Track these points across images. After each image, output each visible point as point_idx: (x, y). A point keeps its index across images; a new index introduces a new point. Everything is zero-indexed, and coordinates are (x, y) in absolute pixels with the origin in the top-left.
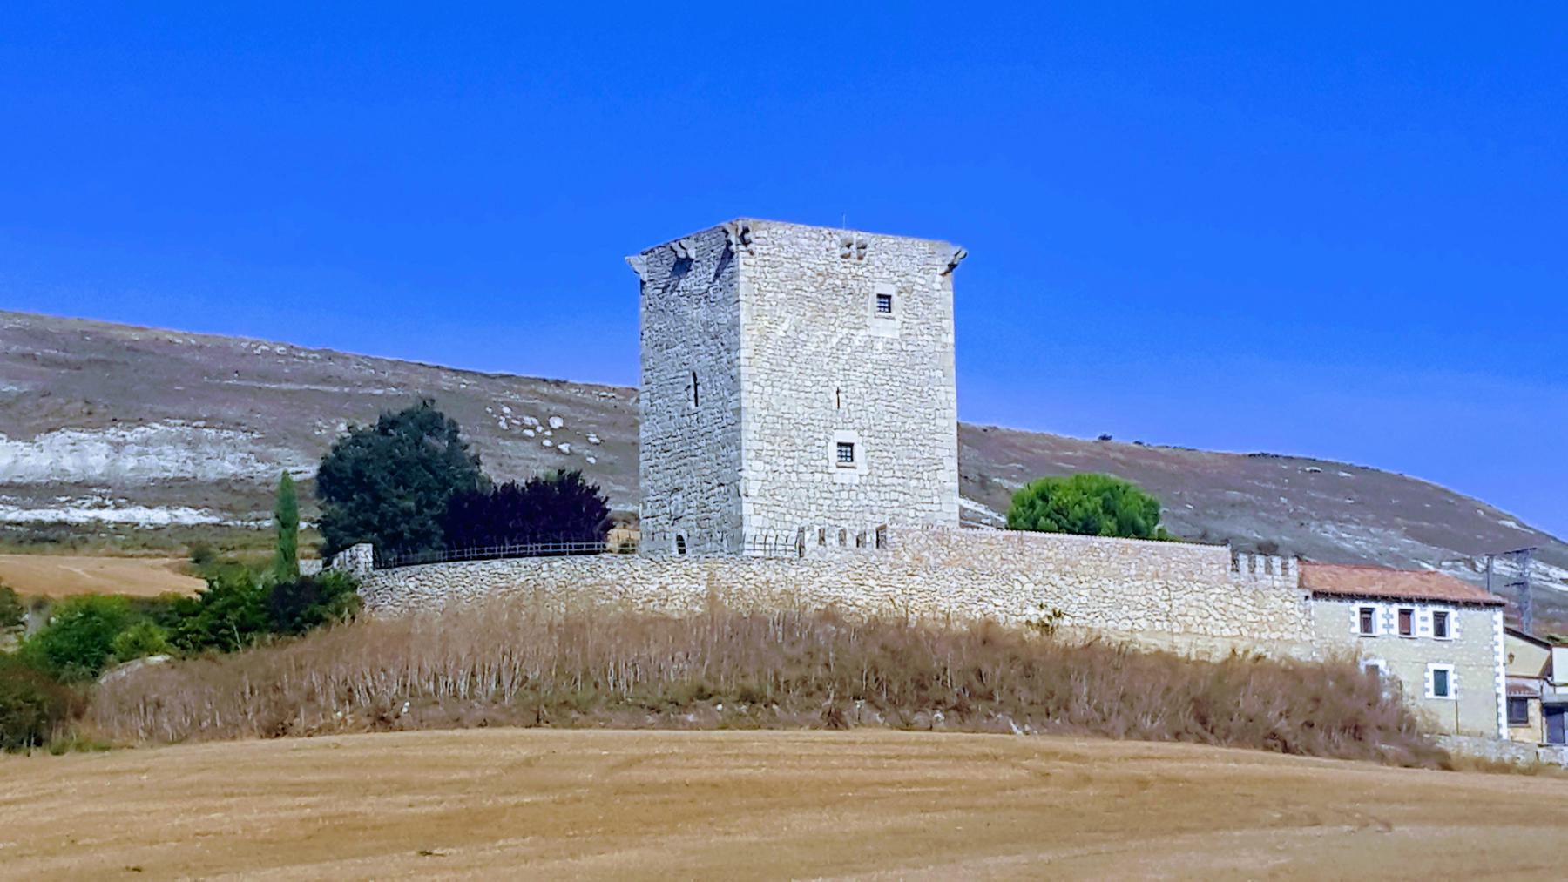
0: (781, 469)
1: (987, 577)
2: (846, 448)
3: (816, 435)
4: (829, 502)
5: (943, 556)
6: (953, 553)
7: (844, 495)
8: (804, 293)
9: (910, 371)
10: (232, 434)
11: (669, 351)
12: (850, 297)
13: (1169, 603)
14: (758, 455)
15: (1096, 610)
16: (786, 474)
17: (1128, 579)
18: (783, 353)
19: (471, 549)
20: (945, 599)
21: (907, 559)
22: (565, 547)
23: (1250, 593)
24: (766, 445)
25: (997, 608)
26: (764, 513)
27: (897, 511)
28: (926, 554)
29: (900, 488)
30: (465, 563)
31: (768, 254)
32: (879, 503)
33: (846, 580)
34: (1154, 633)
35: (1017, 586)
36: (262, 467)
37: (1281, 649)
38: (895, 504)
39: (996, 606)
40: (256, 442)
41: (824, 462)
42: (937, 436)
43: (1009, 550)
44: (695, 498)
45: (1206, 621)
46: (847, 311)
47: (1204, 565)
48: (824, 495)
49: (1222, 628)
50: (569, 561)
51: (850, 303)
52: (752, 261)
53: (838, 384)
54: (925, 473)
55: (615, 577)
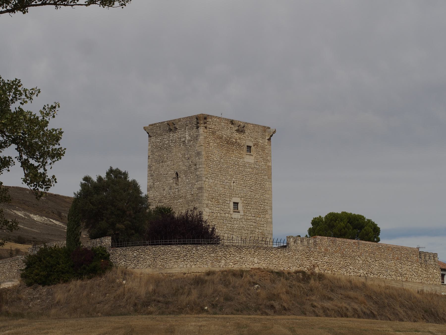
0: (215, 211)
1: (348, 258)
2: (236, 204)
3: (226, 199)
5: (334, 249)
6: (337, 248)
7: (235, 222)
8: (223, 144)
9: (257, 176)
12: (238, 146)
13: (401, 269)
14: (207, 206)
15: (380, 272)
20: (335, 266)
22: (202, 241)
23: (424, 266)
24: (210, 202)
27: (252, 229)
28: (329, 248)
29: (254, 221)
31: (211, 128)
33: (304, 258)
34: (396, 281)
35: (357, 261)
38: (252, 227)
39: (351, 269)
41: (229, 209)
42: (266, 201)
43: (355, 247)
46: (237, 151)
47: (411, 255)
48: (229, 222)
49: (416, 279)
50: (204, 247)
52: (206, 130)
54: (262, 215)
55: (223, 254)
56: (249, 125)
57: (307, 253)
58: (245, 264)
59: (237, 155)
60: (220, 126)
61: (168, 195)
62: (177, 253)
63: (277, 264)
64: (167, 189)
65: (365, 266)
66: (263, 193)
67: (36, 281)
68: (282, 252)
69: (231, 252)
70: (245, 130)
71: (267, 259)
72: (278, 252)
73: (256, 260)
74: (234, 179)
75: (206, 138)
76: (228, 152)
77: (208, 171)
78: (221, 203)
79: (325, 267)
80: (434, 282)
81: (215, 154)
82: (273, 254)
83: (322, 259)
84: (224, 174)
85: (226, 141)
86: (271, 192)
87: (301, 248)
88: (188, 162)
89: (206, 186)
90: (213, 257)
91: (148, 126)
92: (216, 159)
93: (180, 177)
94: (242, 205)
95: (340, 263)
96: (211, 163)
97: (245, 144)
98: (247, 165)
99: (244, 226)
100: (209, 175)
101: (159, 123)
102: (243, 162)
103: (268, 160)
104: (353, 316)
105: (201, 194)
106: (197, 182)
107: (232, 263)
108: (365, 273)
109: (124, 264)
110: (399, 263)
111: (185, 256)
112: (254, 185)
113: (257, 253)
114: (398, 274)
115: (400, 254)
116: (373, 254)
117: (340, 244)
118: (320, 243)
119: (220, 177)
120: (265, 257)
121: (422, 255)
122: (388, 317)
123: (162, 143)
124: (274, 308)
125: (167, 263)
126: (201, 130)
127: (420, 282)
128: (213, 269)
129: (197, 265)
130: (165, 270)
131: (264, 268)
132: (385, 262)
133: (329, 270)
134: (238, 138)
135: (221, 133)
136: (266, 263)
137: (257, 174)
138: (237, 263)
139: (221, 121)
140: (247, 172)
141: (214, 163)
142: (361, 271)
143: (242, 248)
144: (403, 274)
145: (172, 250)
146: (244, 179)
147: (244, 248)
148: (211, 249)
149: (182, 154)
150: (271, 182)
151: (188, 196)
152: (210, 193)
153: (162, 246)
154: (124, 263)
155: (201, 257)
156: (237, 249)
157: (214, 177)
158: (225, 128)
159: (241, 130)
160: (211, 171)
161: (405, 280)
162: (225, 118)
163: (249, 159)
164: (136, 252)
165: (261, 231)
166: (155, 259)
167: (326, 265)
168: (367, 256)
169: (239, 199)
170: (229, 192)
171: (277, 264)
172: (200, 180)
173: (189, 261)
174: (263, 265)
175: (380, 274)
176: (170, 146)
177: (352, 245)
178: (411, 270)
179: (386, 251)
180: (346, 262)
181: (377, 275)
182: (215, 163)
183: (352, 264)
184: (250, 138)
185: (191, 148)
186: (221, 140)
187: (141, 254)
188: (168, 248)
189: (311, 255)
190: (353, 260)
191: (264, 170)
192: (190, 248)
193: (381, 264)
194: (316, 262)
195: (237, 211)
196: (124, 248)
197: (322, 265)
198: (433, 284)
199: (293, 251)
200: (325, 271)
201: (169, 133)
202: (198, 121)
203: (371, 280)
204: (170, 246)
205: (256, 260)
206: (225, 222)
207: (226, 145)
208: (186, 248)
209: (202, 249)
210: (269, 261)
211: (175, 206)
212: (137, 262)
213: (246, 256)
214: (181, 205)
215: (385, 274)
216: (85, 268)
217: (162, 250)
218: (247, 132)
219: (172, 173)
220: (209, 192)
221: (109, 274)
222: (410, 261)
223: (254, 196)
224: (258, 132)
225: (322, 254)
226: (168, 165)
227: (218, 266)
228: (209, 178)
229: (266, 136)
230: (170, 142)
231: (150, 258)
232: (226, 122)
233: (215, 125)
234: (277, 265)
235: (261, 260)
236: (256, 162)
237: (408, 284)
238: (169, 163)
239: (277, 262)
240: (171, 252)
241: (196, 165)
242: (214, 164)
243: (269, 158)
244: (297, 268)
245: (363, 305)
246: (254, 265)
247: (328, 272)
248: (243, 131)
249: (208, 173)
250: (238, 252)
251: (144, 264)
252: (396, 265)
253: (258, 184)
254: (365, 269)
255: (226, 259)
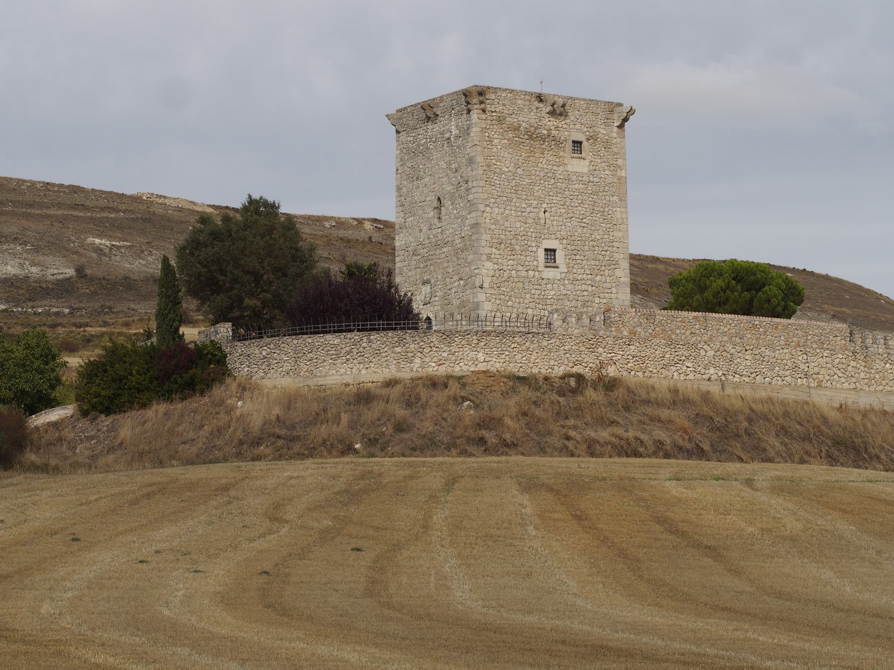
0: (505, 268)
1: (682, 346)
2: (550, 253)
3: (529, 243)
4: (539, 292)
5: (650, 331)
6: (657, 329)
7: (550, 286)
8: (520, 140)
9: (595, 197)
10: (12, 246)
11: (419, 182)
12: (553, 142)
13: (807, 365)
14: (489, 257)
15: (756, 371)
16: (508, 271)
17: (779, 348)
18: (506, 183)
19: (309, 326)
20: (652, 362)
21: (625, 333)
23: (862, 357)
24: (494, 250)
25: (689, 369)
26: (493, 300)
27: (586, 298)
29: (589, 282)
30: (304, 336)
32: (574, 293)
33: (582, 349)
34: (796, 387)
35: (703, 353)
36: (34, 270)
37: (802, 396)
38: (585, 293)
39: (688, 367)
40: (27, 251)
41: (535, 263)
42: (615, 244)
44: (440, 289)
45: (832, 378)
46: (551, 153)
47: (831, 337)
48: (536, 287)
49: (843, 383)
50: (382, 335)
51: (553, 147)
52: (484, 116)
53: (545, 205)
54: (607, 271)
55: (417, 346)
56: (576, 101)
57: (590, 340)
58: (460, 364)
59: (551, 159)
60: (515, 106)
61: (426, 240)
62: (335, 349)
63: (525, 362)
64: (425, 229)
65: (721, 360)
66: (609, 230)
67: (94, 407)
68: (536, 339)
69: (432, 344)
70: (568, 111)
71: (504, 353)
72: (526, 340)
73: (481, 356)
74: (545, 205)
75: (484, 131)
76: (532, 154)
77: (489, 192)
78: (519, 252)
79: (630, 365)
80: (885, 387)
81: (504, 159)
82: (516, 344)
83: (623, 351)
84: (524, 197)
85: (528, 133)
86: (625, 226)
87: (576, 331)
88: (456, 177)
89: (487, 220)
90: (399, 353)
91: (395, 112)
92: (507, 170)
93: (444, 206)
94: (563, 253)
95: (664, 357)
96: (495, 178)
97: (568, 138)
98: (574, 178)
99: (569, 293)
100: (493, 200)
101: (412, 106)
102: (565, 172)
103: (619, 167)
104: (655, 454)
105: (476, 235)
106: (469, 214)
107: (435, 362)
108: (720, 373)
109: (248, 371)
110: (801, 353)
111: (348, 353)
112: (588, 214)
113: (483, 344)
114: (798, 374)
115: (803, 336)
116: (740, 338)
117: (663, 322)
118: (620, 321)
119: (515, 203)
120: (499, 349)
121: (857, 336)
122: (736, 455)
123: (416, 143)
124: (486, 442)
125: (317, 367)
126: (475, 115)
127: (852, 387)
128: (399, 375)
129: (371, 370)
130: (314, 379)
131: (497, 371)
132: (767, 352)
133: (639, 370)
134: (552, 128)
135: (516, 120)
136: (502, 361)
137: (596, 193)
138: (444, 362)
139: (517, 97)
140: (575, 190)
141: (503, 176)
142: (712, 371)
143: (454, 335)
144: (811, 373)
145: (327, 342)
146: (568, 204)
147: (457, 335)
148: (396, 340)
149: (446, 163)
150: (626, 207)
151: (457, 241)
152: (495, 233)
153: (308, 336)
154: (247, 369)
155: (377, 353)
156: (444, 337)
157: (502, 202)
158: (526, 110)
159: (559, 111)
160: (496, 191)
161: (816, 384)
162: (526, 92)
163: (579, 166)
164: (265, 348)
165: (605, 301)
166: (296, 361)
167: (632, 361)
168: (725, 341)
169: (557, 242)
170: (535, 230)
171: (525, 362)
172: (474, 209)
173: (355, 361)
174: (496, 365)
175: (757, 375)
176: (428, 148)
177: (691, 321)
178: (831, 366)
179: (770, 330)
180: (676, 354)
181: (749, 377)
182: (505, 177)
183: (691, 357)
184: (578, 126)
185: (460, 151)
186: (516, 132)
187: (274, 353)
188: (319, 339)
189: (599, 344)
190: (693, 350)
191: (610, 186)
192: (358, 337)
193: (758, 357)
194: (609, 355)
195: (552, 265)
196: (247, 343)
197: (623, 362)
198: (884, 391)
199: (560, 337)
200: (630, 373)
201: (426, 124)
202: (467, 100)
203: (735, 386)
204: (322, 335)
205: (481, 356)
206: (528, 288)
207: (528, 141)
208: (350, 339)
209: (379, 339)
210: (508, 357)
211: (438, 261)
212: (268, 366)
213: (462, 350)
214: (446, 258)
215: (769, 374)
216: (176, 382)
217: (309, 343)
218: (572, 115)
219: (432, 198)
220: (491, 232)
221: (217, 391)
222: (827, 349)
223: (589, 235)
224: (596, 115)
225: (624, 340)
226: (426, 185)
227: (408, 369)
228: (491, 205)
229: (613, 121)
230: (428, 141)
231: (288, 358)
232: (527, 97)
233: (504, 105)
234: (525, 363)
235: (492, 355)
236: (592, 173)
237: (821, 393)
238: (427, 180)
239: (524, 358)
240: (324, 346)
241: (467, 182)
242: (502, 179)
243: (620, 162)
244: (568, 369)
245: (679, 434)
246: (478, 366)
247: (637, 373)
248: (565, 114)
249: (489, 195)
250: (445, 342)
251: (279, 370)
252: (794, 357)
253: (597, 212)
254: (721, 366)
255: (423, 357)
